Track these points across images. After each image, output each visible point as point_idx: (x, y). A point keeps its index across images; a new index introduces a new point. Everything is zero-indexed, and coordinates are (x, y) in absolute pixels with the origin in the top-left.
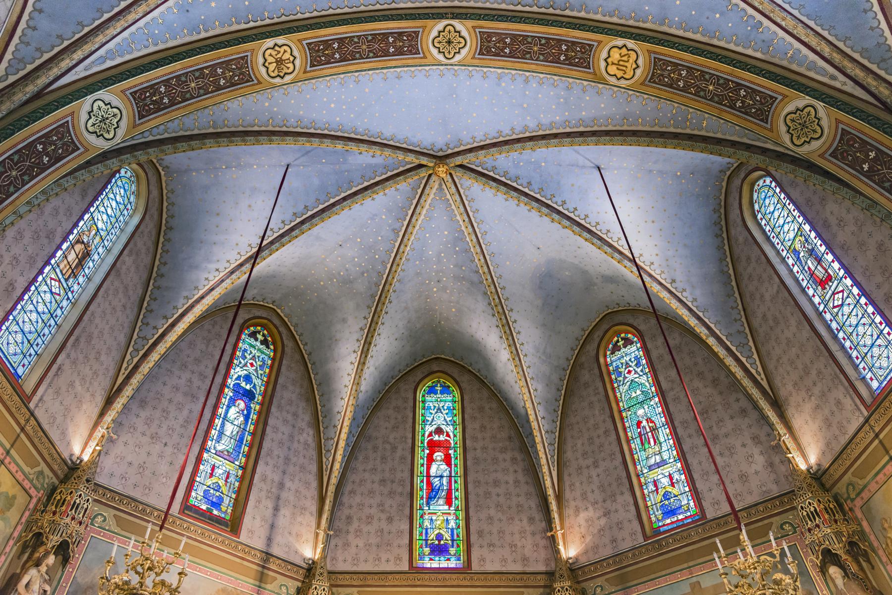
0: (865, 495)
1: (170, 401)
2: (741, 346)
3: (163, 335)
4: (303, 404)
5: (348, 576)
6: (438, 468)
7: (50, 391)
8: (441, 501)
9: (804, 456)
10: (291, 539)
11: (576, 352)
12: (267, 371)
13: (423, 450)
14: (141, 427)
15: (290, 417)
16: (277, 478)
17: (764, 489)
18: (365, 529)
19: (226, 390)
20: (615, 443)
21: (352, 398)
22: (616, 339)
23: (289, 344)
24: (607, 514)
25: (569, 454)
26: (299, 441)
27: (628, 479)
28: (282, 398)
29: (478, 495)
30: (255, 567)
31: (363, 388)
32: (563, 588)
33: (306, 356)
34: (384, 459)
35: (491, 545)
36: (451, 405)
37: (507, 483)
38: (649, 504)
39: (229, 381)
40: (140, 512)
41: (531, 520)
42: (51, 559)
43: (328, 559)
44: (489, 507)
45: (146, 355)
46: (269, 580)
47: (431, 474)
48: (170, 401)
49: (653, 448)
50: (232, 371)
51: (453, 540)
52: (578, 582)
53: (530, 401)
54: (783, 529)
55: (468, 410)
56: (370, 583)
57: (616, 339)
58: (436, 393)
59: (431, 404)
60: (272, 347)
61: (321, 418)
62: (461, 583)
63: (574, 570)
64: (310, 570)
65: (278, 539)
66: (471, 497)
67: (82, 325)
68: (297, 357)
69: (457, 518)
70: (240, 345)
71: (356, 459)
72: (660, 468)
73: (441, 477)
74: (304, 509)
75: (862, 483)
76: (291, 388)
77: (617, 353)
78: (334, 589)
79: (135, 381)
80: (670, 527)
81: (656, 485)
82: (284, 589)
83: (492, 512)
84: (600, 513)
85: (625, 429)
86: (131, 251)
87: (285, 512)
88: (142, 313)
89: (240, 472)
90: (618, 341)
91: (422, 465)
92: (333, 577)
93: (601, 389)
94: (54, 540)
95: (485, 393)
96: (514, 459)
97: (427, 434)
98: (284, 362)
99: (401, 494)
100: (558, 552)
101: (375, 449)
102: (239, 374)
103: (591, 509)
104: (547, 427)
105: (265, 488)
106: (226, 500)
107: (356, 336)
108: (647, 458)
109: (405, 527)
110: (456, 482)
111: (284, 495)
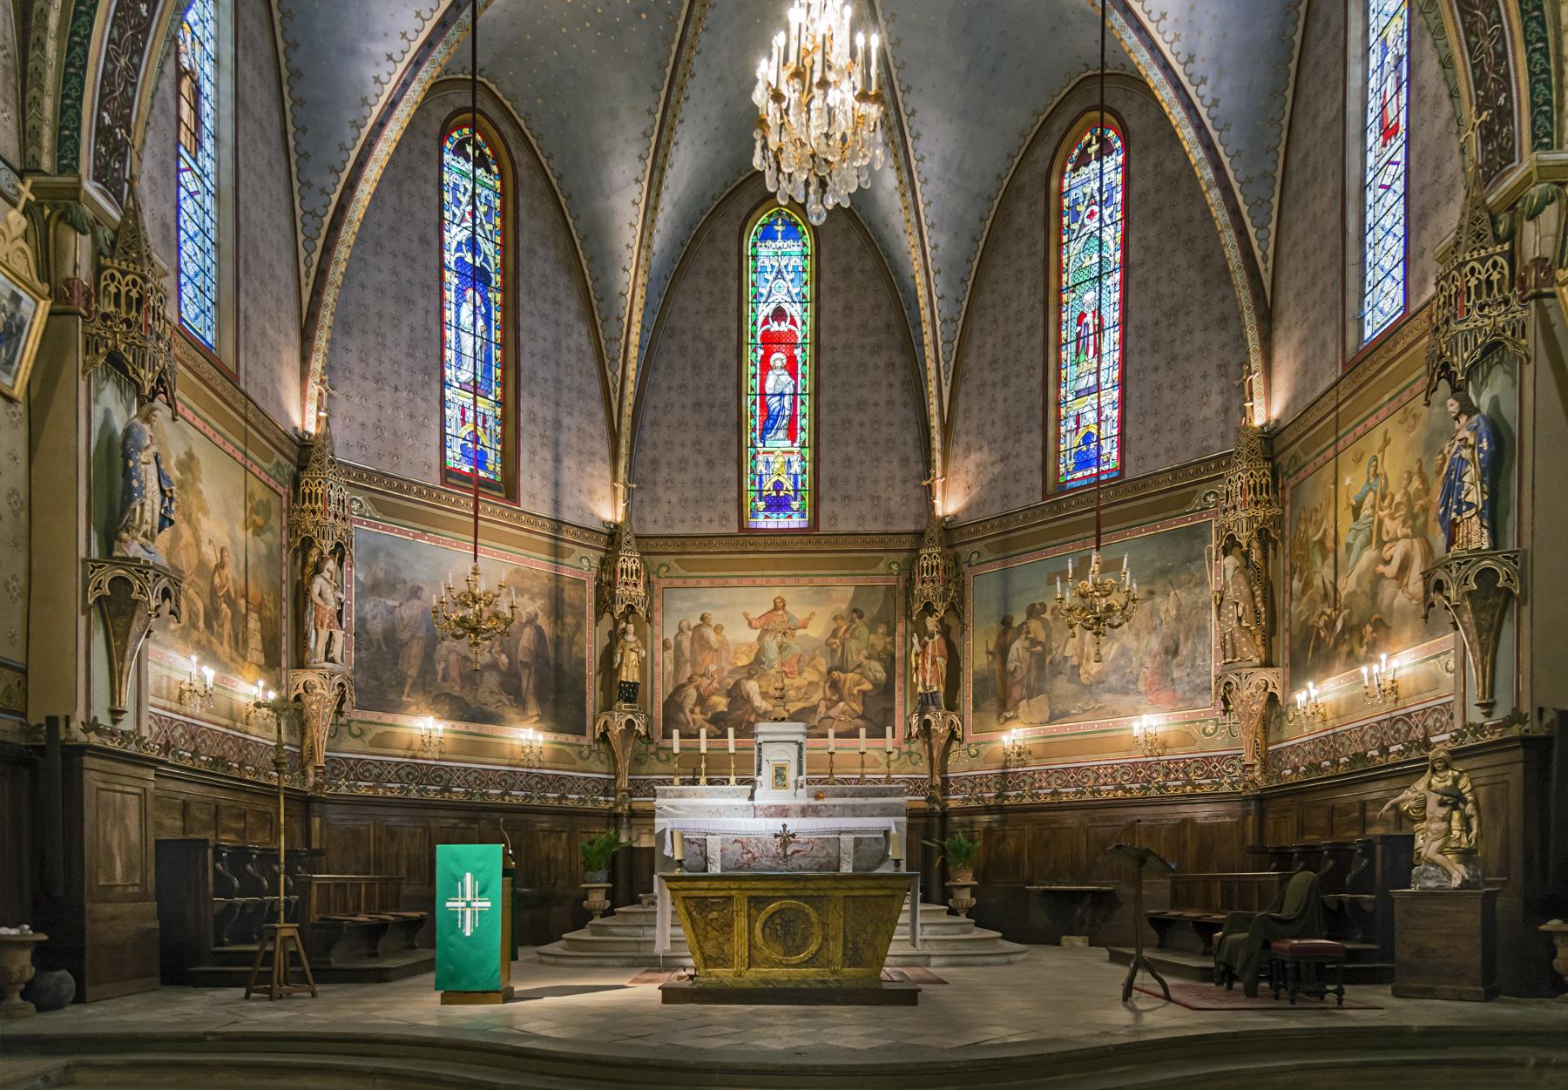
0: (1301, 474)
1: (380, 315)
2: (1258, 204)
3: (342, 208)
4: (563, 280)
5: (661, 542)
6: (777, 380)
7: (250, 354)
8: (781, 434)
9: (1268, 404)
10: (583, 498)
11: (1016, 161)
12: (498, 221)
13: (755, 351)
14: (358, 369)
15: (548, 308)
16: (549, 415)
17: (1205, 444)
18: (678, 477)
19: (447, 274)
20: (1039, 350)
21: (640, 272)
22: (1087, 137)
23: (522, 157)
24: (1004, 459)
25: (972, 360)
26: (569, 350)
27: (1042, 409)
28: (532, 275)
29: (832, 425)
30: (547, 540)
31: (656, 248)
33: (554, 181)
34: (696, 367)
35: (846, 497)
36: (799, 262)
37: (876, 404)
38: (1062, 448)
39: (447, 255)
40: (396, 489)
41: (904, 461)
42: (331, 565)
43: (634, 521)
44: (847, 444)
45: (328, 250)
47: (768, 391)
48: (380, 315)
49: (1089, 362)
50: (447, 234)
51: (796, 490)
53: (922, 273)
55: (826, 276)
57: (1087, 137)
58: (775, 239)
59: (767, 263)
60: (495, 168)
61: (595, 302)
63: (950, 531)
64: (613, 535)
65: (568, 500)
66: (824, 428)
67: (242, 233)
68: (540, 184)
69: (803, 459)
70: (446, 176)
71: (656, 369)
72: (1090, 400)
73: (782, 395)
74: (592, 454)
75: (1304, 459)
76: (541, 252)
77: (1083, 169)
78: (646, 558)
79: (330, 296)
80: (1079, 484)
81: (1078, 422)
82: (585, 562)
83: (851, 450)
84: (995, 456)
85: (1059, 324)
86: (244, 47)
87: (569, 462)
88: (293, 162)
89: (499, 410)
90: (1089, 144)
91: (754, 376)
93: (1040, 247)
94: (328, 545)
95: (856, 239)
96: (890, 365)
97: (759, 323)
98: (522, 201)
99: (724, 425)
100: (933, 506)
101: (683, 350)
102: (458, 238)
103: (986, 448)
104: (945, 312)
105: (537, 431)
106: (491, 455)
107: (635, 150)
108: (1078, 377)
109: (732, 474)
110: (803, 403)
111: (564, 438)
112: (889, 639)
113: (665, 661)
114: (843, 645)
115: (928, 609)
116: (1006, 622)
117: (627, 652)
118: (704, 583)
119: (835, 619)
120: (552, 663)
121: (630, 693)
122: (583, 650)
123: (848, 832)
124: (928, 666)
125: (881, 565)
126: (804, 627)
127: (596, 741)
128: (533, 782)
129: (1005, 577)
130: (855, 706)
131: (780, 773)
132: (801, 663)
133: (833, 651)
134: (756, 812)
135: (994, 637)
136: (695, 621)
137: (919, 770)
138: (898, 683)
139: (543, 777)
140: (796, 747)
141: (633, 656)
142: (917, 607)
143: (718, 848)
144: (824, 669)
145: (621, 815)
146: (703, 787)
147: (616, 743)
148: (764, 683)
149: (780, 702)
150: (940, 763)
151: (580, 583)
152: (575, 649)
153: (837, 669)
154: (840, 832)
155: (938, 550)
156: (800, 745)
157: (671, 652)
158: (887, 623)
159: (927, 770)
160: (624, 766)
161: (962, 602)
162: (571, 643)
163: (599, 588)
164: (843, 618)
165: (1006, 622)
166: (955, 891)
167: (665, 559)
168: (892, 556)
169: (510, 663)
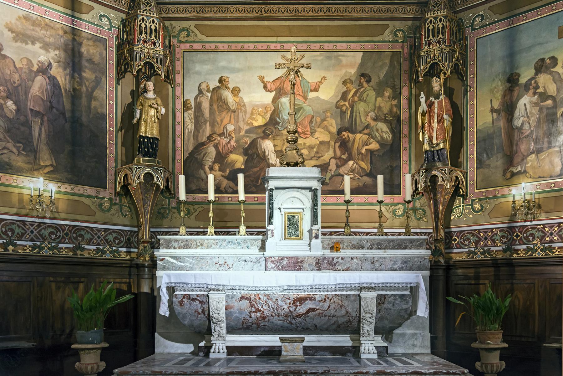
32: (436, 18)
46: (84, 9)
52: (456, 13)
54: (481, 206)
56: (208, 15)
62: (316, 15)
78: (167, 23)
82: (105, 20)
92: (164, 8)
112: (394, 102)
113: (187, 120)
114: (352, 107)
115: (434, 70)
116: (512, 80)
117: (146, 108)
118: (222, 47)
119: (345, 83)
120: (68, 115)
121: (151, 148)
122: (103, 106)
123: (370, 288)
124: (435, 125)
125: (387, 32)
126: (316, 90)
127: (117, 194)
128: (46, 233)
129: (511, 37)
130: (363, 165)
131: (292, 223)
132: (314, 124)
133: (343, 113)
134: (270, 264)
135: (499, 95)
136: (214, 84)
137: (423, 224)
138: (404, 144)
139: (59, 228)
140: (310, 194)
141: (152, 112)
142: (423, 69)
143: (222, 305)
144: (334, 130)
145: (143, 266)
146: (210, 238)
147: (137, 197)
148: (278, 142)
149: (292, 146)
150: (443, 219)
151: (99, 41)
152: (94, 104)
153: (346, 129)
154: (361, 289)
155: (444, 13)
156: (314, 191)
157: (192, 112)
158: (393, 88)
159: (431, 223)
160: (145, 218)
161: (465, 64)
162: (90, 97)
163: (119, 48)
164: (352, 82)
165: (512, 80)
166: (483, 354)
167: (185, 24)
168: (397, 24)
169: (18, 110)
